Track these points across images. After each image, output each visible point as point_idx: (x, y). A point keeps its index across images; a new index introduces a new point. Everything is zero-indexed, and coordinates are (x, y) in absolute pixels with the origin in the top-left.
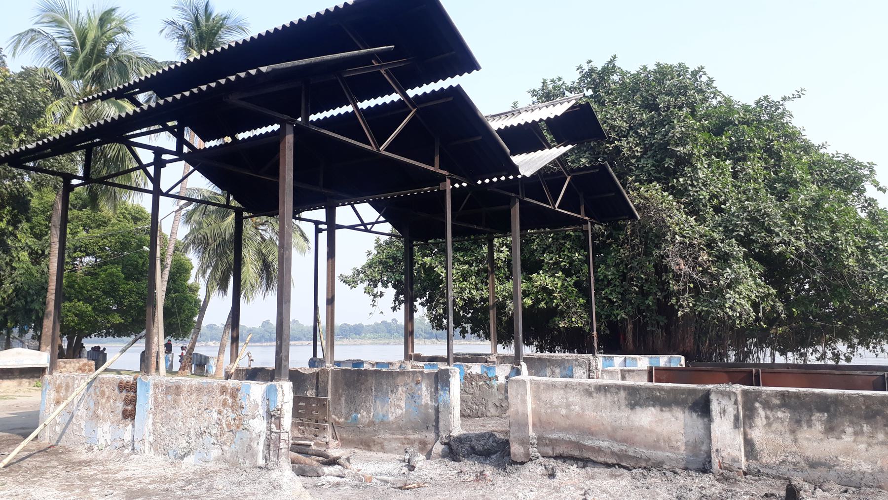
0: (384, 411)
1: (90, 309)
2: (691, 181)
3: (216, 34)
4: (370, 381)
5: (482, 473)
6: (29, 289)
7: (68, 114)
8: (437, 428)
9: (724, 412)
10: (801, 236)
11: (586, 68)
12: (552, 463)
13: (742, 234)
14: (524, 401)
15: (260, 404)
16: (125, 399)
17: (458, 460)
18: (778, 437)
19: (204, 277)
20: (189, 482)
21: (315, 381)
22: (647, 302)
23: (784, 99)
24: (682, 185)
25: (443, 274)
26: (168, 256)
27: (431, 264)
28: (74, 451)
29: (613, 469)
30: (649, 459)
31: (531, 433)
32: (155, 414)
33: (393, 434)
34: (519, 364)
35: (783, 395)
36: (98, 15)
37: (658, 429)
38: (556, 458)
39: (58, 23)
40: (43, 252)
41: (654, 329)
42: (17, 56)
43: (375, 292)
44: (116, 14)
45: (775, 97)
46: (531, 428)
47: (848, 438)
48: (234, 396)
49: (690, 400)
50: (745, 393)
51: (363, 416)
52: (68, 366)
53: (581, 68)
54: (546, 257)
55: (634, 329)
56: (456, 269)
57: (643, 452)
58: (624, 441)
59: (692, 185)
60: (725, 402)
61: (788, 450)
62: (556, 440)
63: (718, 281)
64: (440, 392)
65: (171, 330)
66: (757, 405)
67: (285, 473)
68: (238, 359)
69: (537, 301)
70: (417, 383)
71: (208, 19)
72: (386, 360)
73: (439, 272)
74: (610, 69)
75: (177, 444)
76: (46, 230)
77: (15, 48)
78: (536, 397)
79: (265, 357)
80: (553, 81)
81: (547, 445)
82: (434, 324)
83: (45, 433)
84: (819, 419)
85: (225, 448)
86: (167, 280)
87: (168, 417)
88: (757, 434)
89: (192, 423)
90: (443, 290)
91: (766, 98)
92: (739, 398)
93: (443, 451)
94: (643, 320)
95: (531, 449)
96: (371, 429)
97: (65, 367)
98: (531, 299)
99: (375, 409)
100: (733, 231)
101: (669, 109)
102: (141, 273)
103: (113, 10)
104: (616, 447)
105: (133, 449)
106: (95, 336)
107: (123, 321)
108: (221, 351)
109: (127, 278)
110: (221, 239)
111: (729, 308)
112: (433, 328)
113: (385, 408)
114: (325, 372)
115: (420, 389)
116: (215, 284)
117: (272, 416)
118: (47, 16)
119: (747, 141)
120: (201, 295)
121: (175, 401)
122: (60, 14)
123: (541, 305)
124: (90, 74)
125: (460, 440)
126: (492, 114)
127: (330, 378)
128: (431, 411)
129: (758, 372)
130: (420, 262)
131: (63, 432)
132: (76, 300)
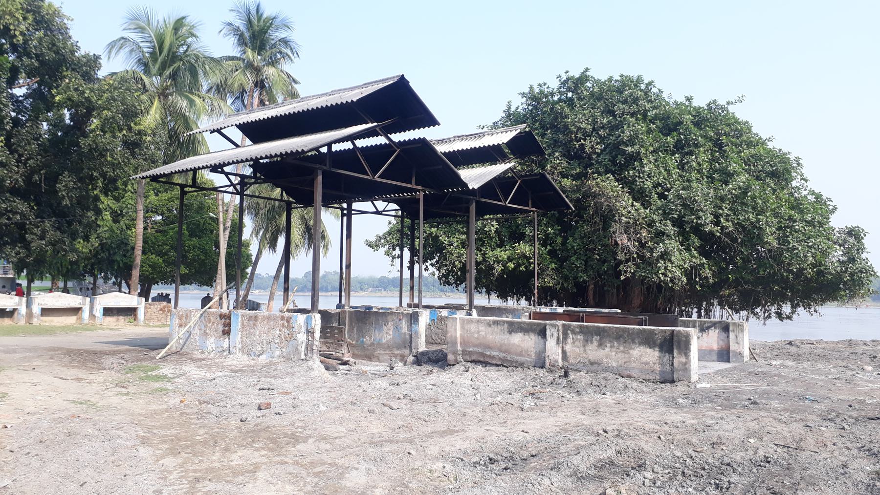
0: (380, 337)
1: (161, 261)
2: (639, 173)
3: (266, 32)
4: (372, 318)
5: (431, 371)
6: (111, 243)
7: (151, 107)
8: (411, 347)
9: (552, 335)
10: (730, 218)
11: (564, 77)
12: (469, 364)
13: (676, 216)
14: (455, 330)
15: (303, 326)
16: (224, 324)
17: (421, 365)
18: (578, 349)
19: (257, 237)
20: (264, 367)
21: (338, 318)
22: (603, 268)
23: (728, 103)
24: (631, 177)
25: (446, 242)
26: (228, 220)
27: (436, 234)
28: (192, 354)
29: (499, 367)
30: (517, 362)
31: (459, 348)
32: (242, 332)
33: (385, 351)
34: (471, 310)
35: (581, 327)
36: (172, 22)
37: (522, 345)
38: (471, 362)
39: (141, 29)
40: (121, 211)
41: (610, 289)
42: (111, 59)
43: (393, 255)
44: (188, 20)
45: (722, 102)
46: (459, 345)
47: (607, 349)
48: (288, 322)
49: (538, 329)
50: (564, 325)
51: (367, 340)
52: (152, 307)
53: (560, 77)
54: (528, 231)
55: (595, 288)
56: (457, 238)
57: (515, 358)
58: (505, 352)
59: (639, 177)
60: (553, 330)
61: (581, 356)
62: (471, 351)
63: (652, 253)
64: (413, 325)
65: (231, 278)
66: (569, 332)
67: (316, 363)
68: (288, 303)
69: (518, 266)
70: (400, 320)
71: (259, 19)
72: (388, 307)
73: (443, 240)
74: (583, 78)
75: (255, 349)
76: (123, 193)
77: (110, 52)
78: (462, 327)
79: (305, 302)
80: (540, 85)
81: (467, 355)
82: (442, 281)
83: (173, 345)
84: (596, 338)
85: (283, 350)
86: (227, 239)
87: (250, 334)
88: (568, 347)
89: (264, 337)
90: (446, 255)
91: (715, 102)
92: (560, 328)
93: (413, 360)
94: (601, 282)
95: (458, 357)
96: (372, 348)
97: (150, 308)
98: (514, 264)
99: (375, 335)
100: (669, 214)
101: (623, 114)
102: (202, 231)
103: (183, 18)
104: (502, 355)
105: (229, 352)
106: (162, 283)
107: (188, 272)
108: (271, 298)
109: (191, 236)
110: (271, 206)
111: (662, 274)
112: (441, 284)
113: (381, 335)
114: (344, 312)
115: (402, 323)
116: (266, 242)
117: (309, 332)
118: (134, 23)
119: (693, 139)
120: (253, 250)
121: (254, 325)
122: (144, 22)
123: (521, 269)
124: (168, 73)
125: (423, 353)
126: (467, 134)
127: (347, 316)
128: (408, 337)
129: (583, 315)
130: (428, 232)
131: (185, 344)
132: (150, 253)
